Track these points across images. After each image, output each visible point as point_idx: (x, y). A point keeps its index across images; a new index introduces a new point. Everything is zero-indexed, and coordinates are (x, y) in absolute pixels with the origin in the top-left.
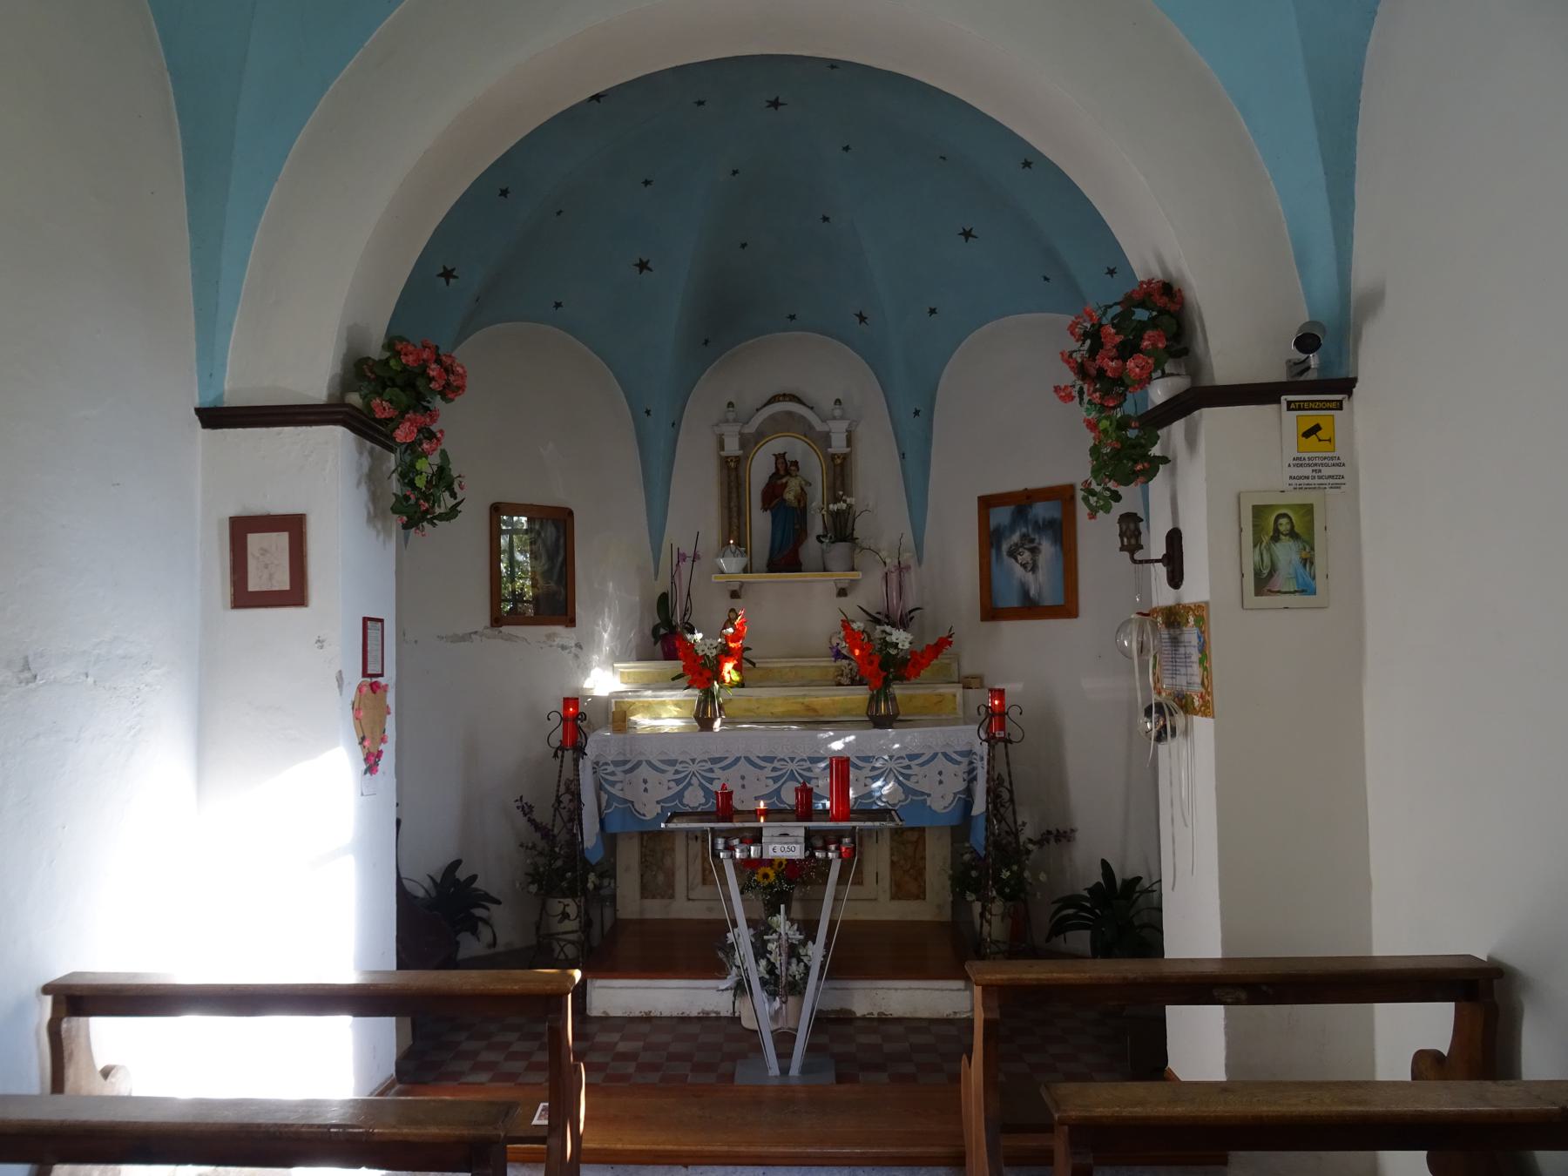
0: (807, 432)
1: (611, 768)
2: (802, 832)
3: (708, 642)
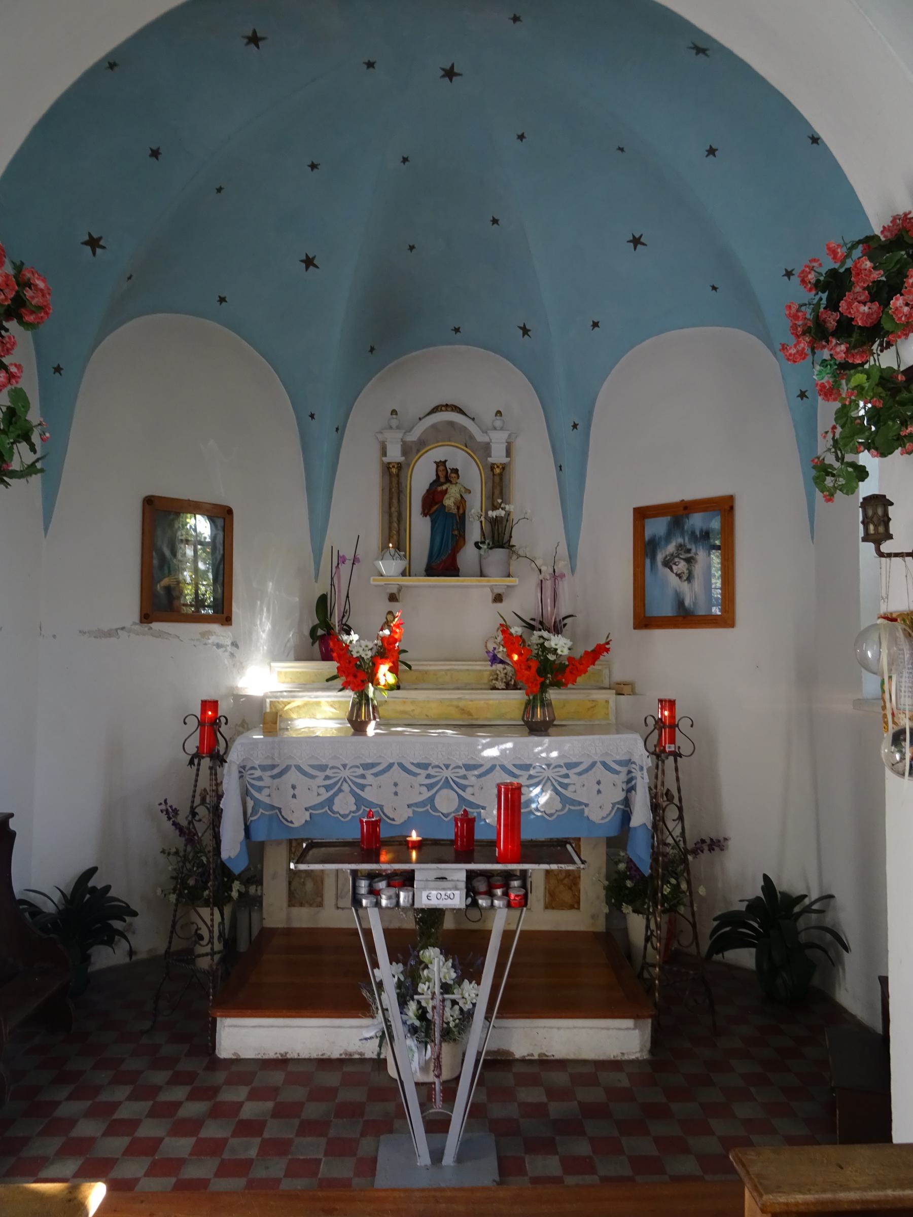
0: (468, 443)
1: (258, 773)
2: (463, 876)
3: (364, 643)
